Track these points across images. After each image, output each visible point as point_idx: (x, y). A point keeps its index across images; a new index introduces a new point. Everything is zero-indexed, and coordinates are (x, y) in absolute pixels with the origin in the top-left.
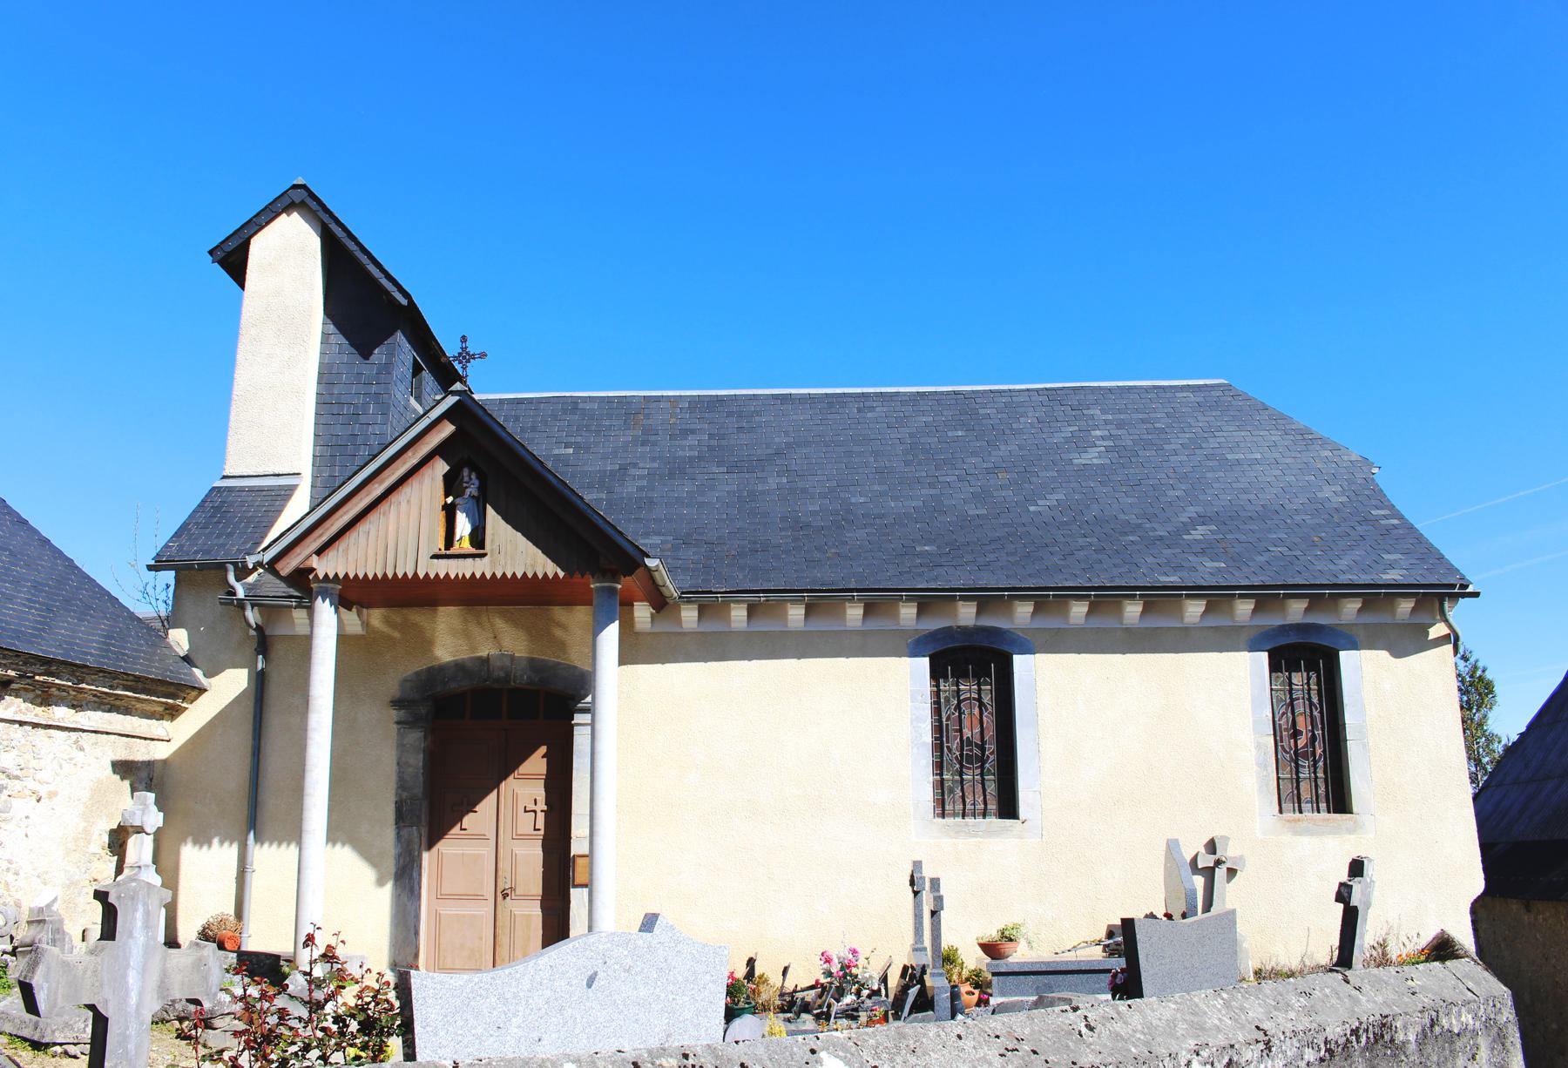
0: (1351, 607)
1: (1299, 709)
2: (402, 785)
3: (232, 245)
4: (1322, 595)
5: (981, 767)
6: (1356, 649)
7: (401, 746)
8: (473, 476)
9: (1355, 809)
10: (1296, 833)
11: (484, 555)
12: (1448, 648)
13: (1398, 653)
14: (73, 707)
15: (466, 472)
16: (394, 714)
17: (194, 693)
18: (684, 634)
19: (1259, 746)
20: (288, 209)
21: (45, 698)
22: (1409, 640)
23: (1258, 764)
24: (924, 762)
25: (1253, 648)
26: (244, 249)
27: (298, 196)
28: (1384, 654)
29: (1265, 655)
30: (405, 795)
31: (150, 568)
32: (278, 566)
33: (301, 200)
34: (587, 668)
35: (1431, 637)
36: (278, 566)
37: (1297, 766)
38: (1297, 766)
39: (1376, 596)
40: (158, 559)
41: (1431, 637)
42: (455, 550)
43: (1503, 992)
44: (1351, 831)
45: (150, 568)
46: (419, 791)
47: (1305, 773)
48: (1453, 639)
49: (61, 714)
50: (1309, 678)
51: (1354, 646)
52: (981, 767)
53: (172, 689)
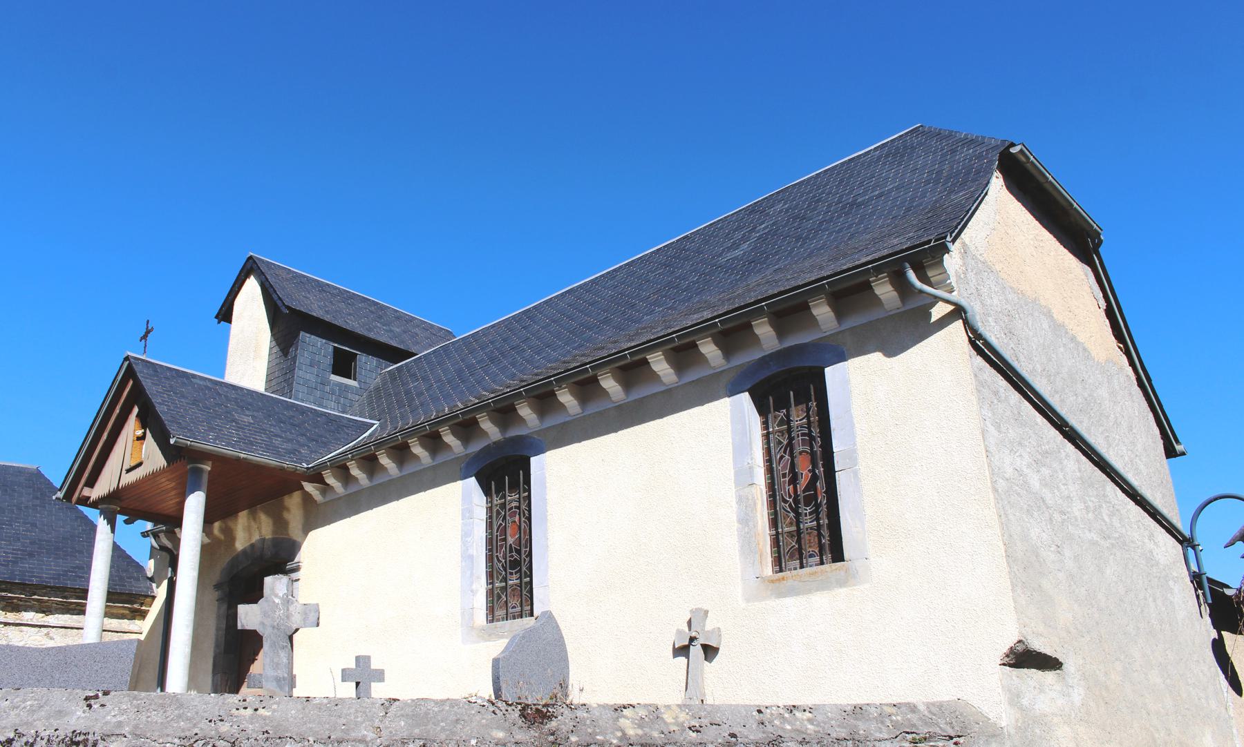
0: (822, 311)
1: (799, 448)
4: (789, 311)
6: (845, 360)
9: (846, 556)
10: (781, 595)
12: (958, 325)
13: (891, 351)
14: (43, 612)
17: (148, 600)
18: (340, 498)
20: (247, 276)
21: (46, 610)
22: (909, 326)
23: (739, 521)
25: (732, 392)
28: (877, 357)
29: (745, 397)
33: (251, 268)
34: (299, 540)
35: (933, 319)
37: (798, 515)
38: (798, 515)
39: (849, 292)
41: (933, 319)
44: (842, 583)
47: (808, 523)
48: (959, 312)
49: (28, 616)
50: (808, 409)
51: (842, 357)
53: (124, 597)
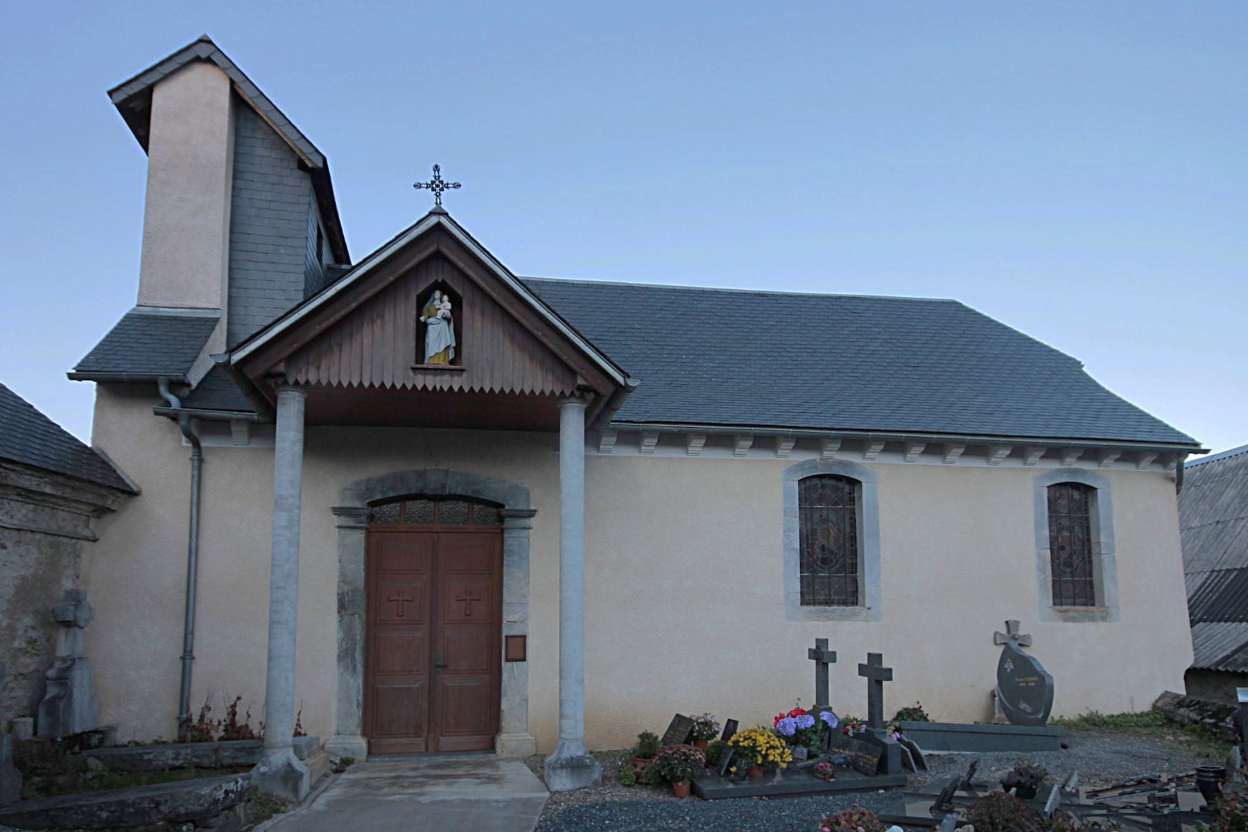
2: (344, 579)
3: (136, 88)
5: (831, 563)
7: (342, 545)
8: (446, 298)
10: (1065, 620)
11: (463, 370)
15: (437, 294)
16: (337, 520)
19: (1039, 556)
23: (1039, 570)
24: (793, 563)
26: (147, 95)
27: (203, 51)
30: (346, 588)
31: (71, 376)
32: (246, 370)
36: (246, 370)
40: (79, 368)
42: (428, 363)
43: (814, 703)
45: (71, 376)
46: (361, 583)
52: (831, 563)
